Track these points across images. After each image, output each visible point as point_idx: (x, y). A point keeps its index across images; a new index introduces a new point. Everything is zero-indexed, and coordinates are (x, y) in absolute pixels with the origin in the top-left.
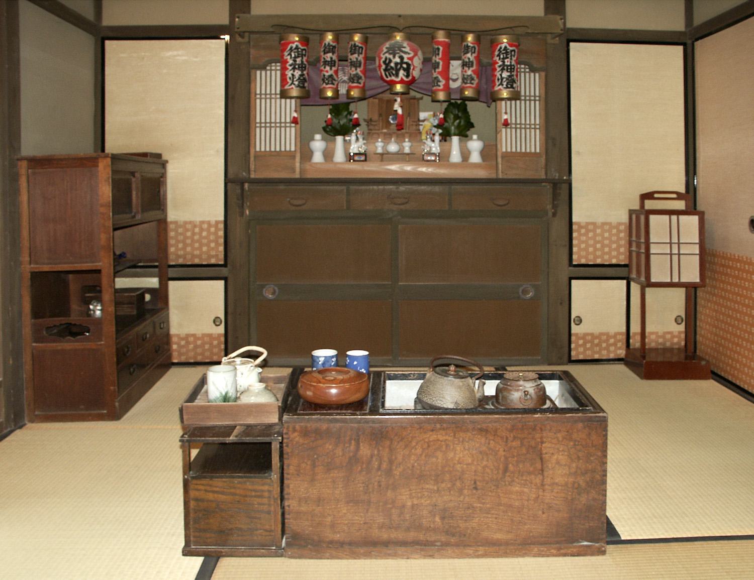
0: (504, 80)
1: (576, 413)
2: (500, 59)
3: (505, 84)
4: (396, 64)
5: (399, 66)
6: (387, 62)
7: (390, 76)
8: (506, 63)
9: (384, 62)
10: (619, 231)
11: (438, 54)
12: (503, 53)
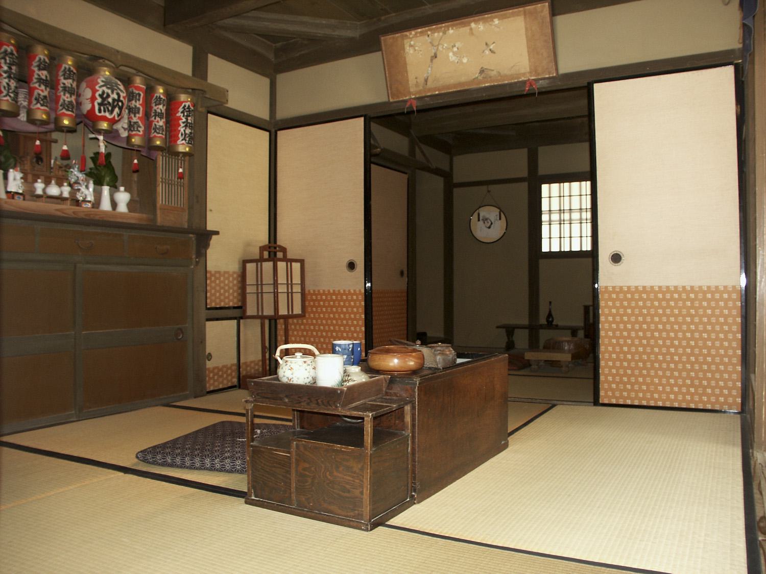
0: (187, 135)
1: (416, 439)
2: (183, 116)
3: (187, 139)
4: (114, 100)
5: (116, 103)
6: (105, 96)
7: (105, 111)
8: (189, 121)
9: (101, 96)
10: (234, 279)
11: (139, 100)
12: (187, 111)
